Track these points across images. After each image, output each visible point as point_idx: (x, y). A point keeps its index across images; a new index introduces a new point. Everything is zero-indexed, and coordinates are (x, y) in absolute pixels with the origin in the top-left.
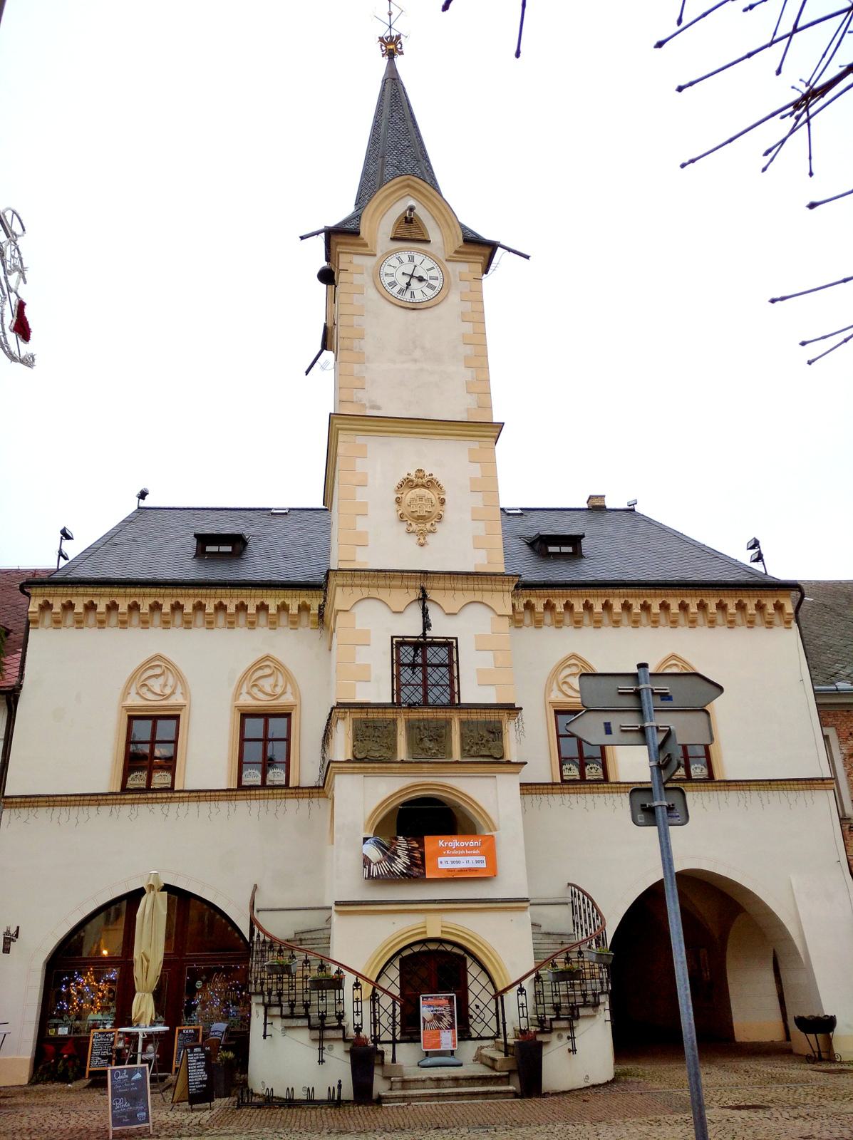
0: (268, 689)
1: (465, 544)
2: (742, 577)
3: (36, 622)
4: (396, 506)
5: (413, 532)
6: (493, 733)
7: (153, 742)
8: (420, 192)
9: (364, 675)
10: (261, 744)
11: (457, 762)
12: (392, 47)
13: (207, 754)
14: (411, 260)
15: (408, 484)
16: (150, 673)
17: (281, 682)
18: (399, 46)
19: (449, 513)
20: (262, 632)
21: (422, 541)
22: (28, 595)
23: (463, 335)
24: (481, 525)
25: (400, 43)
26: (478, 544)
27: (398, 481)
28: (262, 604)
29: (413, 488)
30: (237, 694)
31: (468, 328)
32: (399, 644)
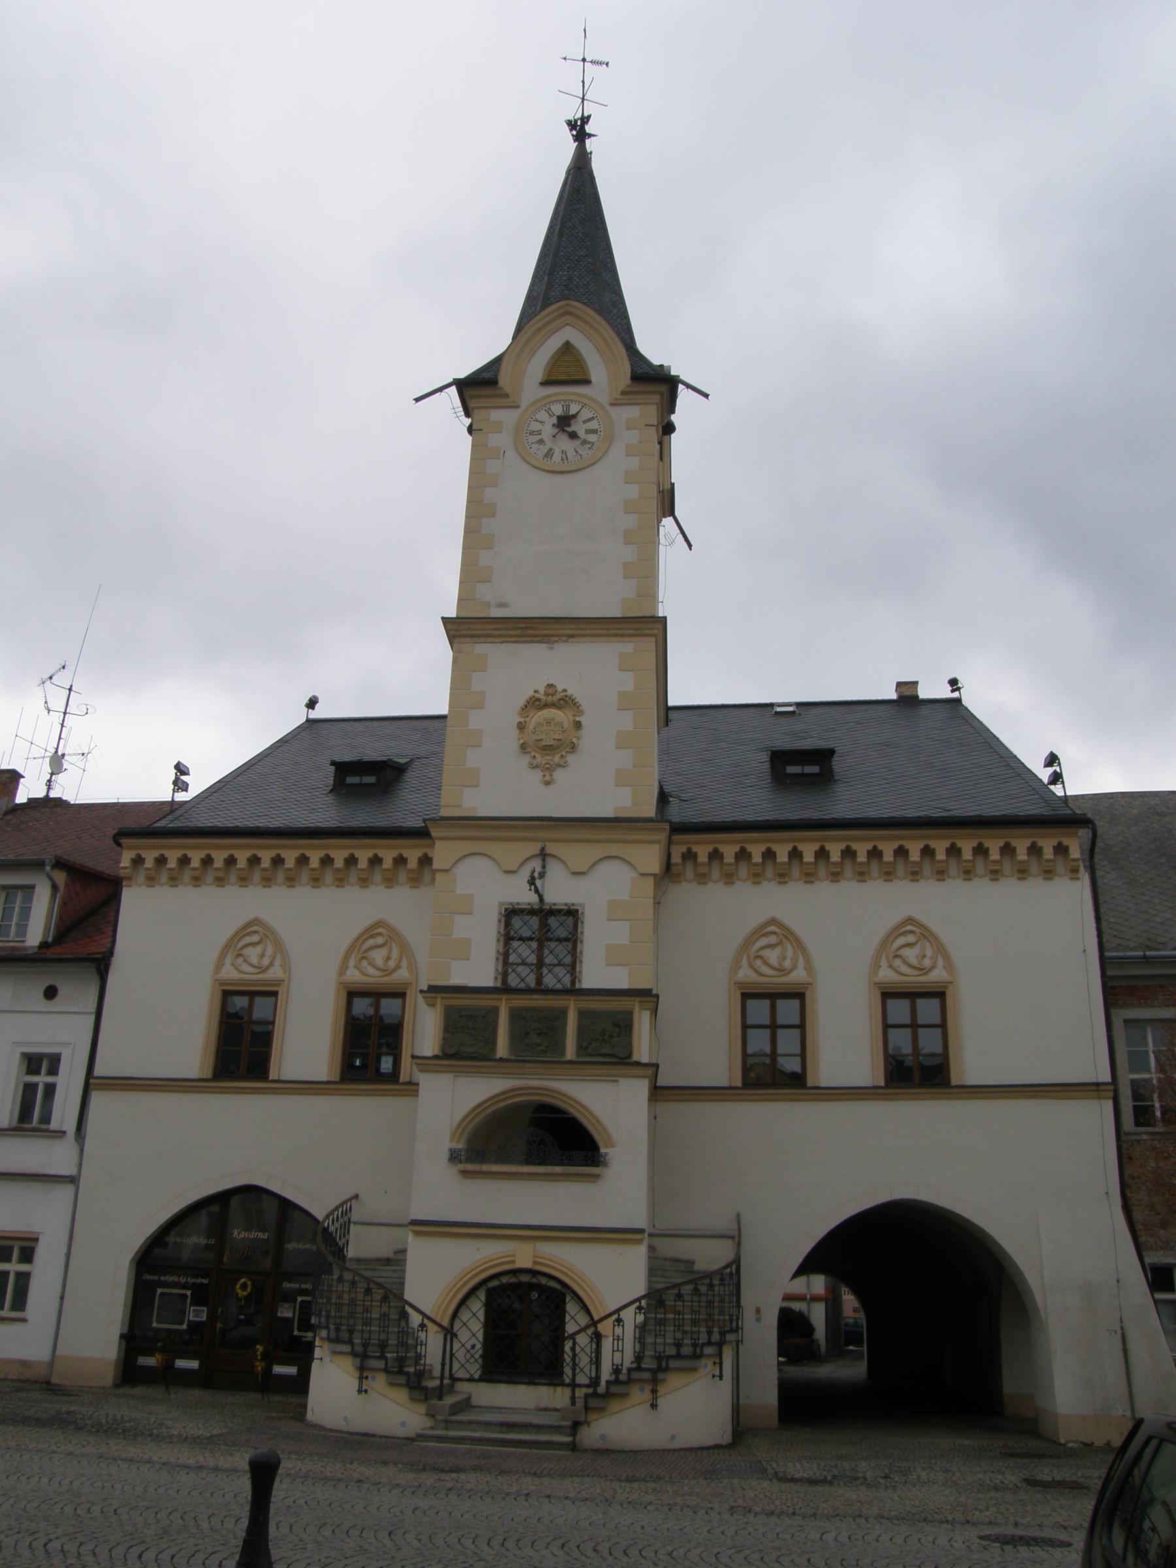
0: (913, 961)
1: (607, 777)
3: (129, 879)
4: (517, 732)
5: (536, 767)
6: (619, 1026)
9: (463, 950)
11: (570, 1062)
13: (307, 1040)
15: (534, 704)
16: (247, 940)
17: (395, 954)
19: (588, 740)
21: (548, 778)
22: (119, 845)
26: (622, 778)
27: (522, 702)
28: (376, 856)
31: (485, 558)
32: (511, 913)
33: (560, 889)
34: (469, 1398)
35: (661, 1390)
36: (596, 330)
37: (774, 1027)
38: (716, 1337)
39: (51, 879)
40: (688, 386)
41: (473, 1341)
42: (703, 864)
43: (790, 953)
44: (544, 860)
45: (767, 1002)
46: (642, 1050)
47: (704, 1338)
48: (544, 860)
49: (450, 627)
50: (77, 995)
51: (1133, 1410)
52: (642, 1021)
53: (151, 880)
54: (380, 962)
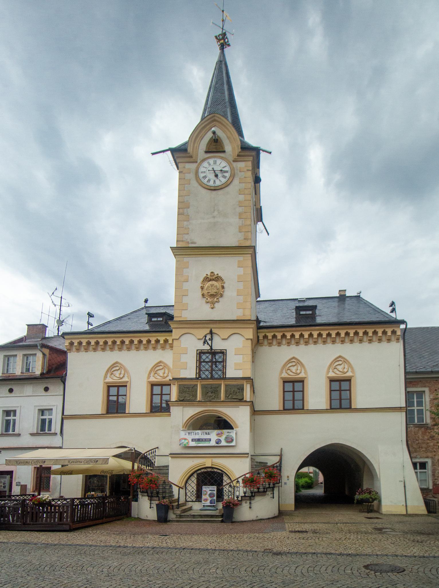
2: (381, 318)
7: (118, 396)
8: (222, 124)
10: (164, 393)
11: (223, 401)
12: (222, 41)
13: (138, 399)
14: (215, 163)
15: (207, 279)
16: (115, 369)
18: (226, 40)
20: (159, 351)
21: (212, 306)
23: (240, 202)
24: (241, 298)
25: (227, 38)
27: (202, 279)
29: (209, 281)
30: (149, 377)
32: (200, 353)
33: (218, 344)
34: (191, 507)
35: (252, 502)
36: (227, 128)
37: (294, 391)
38: (271, 485)
39: (41, 351)
40: (263, 151)
41: (193, 490)
42: (270, 339)
43: (299, 368)
44: (212, 335)
45: (291, 384)
46: (247, 395)
47: (267, 486)
48: (212, 335)
49: (174, 251)
50: (56, 389)
51: (66, 318)
52: (247, 389)
53: (78, 350)
54: (162, 375)
